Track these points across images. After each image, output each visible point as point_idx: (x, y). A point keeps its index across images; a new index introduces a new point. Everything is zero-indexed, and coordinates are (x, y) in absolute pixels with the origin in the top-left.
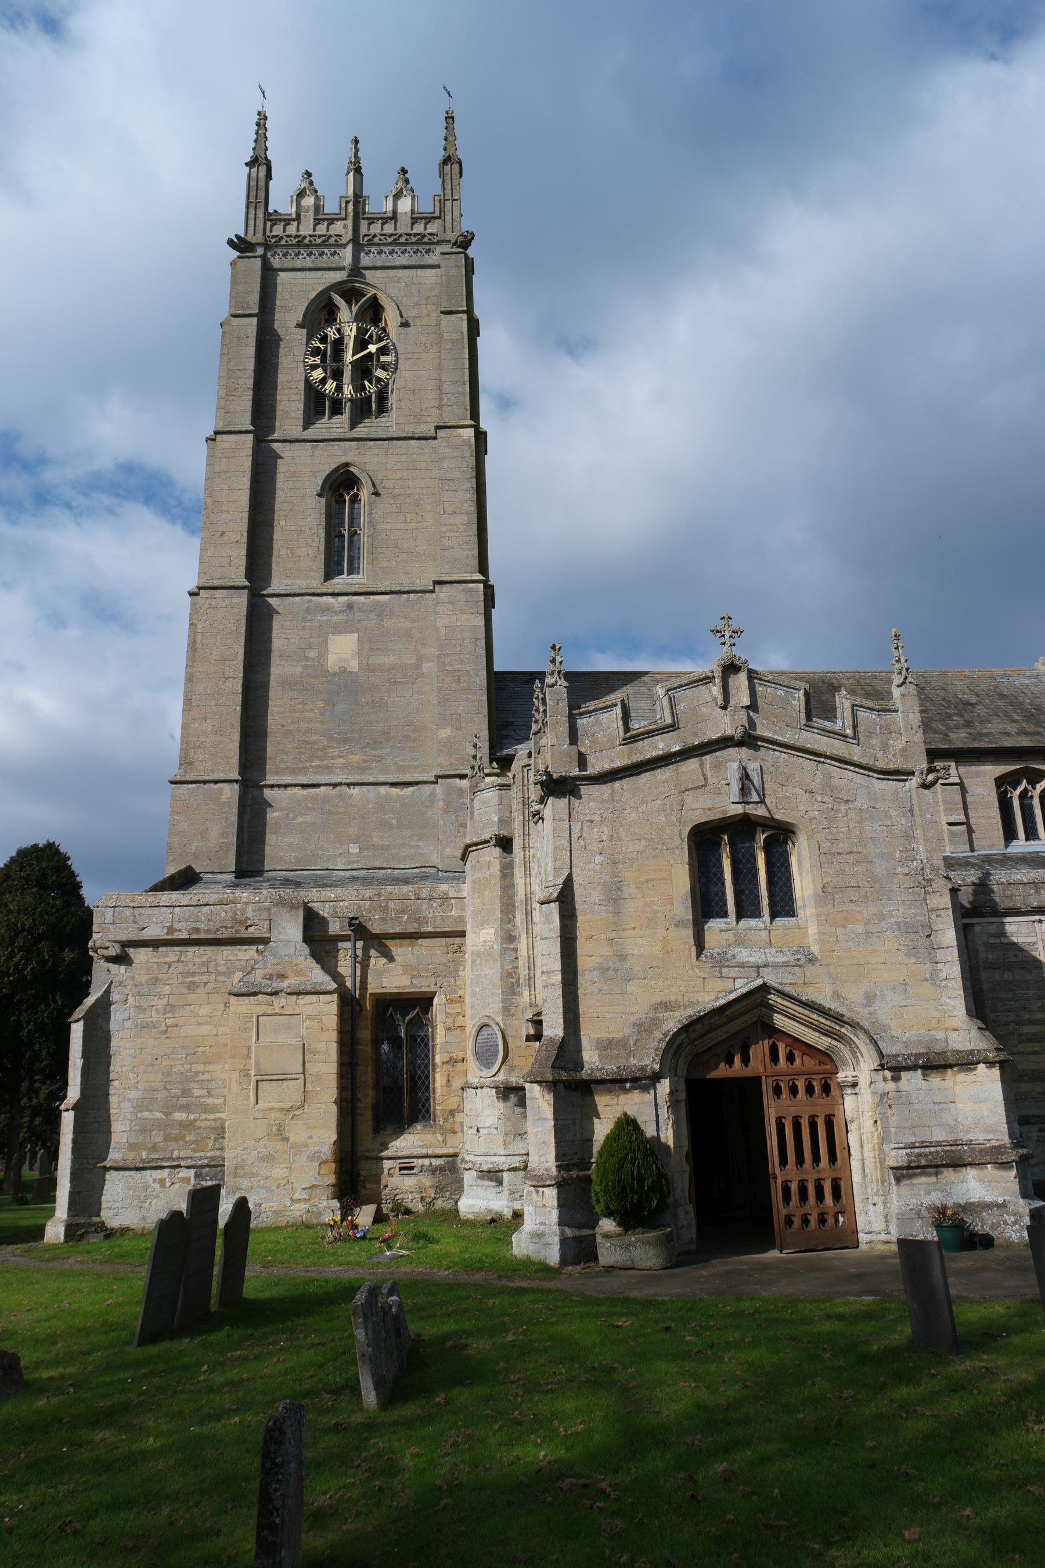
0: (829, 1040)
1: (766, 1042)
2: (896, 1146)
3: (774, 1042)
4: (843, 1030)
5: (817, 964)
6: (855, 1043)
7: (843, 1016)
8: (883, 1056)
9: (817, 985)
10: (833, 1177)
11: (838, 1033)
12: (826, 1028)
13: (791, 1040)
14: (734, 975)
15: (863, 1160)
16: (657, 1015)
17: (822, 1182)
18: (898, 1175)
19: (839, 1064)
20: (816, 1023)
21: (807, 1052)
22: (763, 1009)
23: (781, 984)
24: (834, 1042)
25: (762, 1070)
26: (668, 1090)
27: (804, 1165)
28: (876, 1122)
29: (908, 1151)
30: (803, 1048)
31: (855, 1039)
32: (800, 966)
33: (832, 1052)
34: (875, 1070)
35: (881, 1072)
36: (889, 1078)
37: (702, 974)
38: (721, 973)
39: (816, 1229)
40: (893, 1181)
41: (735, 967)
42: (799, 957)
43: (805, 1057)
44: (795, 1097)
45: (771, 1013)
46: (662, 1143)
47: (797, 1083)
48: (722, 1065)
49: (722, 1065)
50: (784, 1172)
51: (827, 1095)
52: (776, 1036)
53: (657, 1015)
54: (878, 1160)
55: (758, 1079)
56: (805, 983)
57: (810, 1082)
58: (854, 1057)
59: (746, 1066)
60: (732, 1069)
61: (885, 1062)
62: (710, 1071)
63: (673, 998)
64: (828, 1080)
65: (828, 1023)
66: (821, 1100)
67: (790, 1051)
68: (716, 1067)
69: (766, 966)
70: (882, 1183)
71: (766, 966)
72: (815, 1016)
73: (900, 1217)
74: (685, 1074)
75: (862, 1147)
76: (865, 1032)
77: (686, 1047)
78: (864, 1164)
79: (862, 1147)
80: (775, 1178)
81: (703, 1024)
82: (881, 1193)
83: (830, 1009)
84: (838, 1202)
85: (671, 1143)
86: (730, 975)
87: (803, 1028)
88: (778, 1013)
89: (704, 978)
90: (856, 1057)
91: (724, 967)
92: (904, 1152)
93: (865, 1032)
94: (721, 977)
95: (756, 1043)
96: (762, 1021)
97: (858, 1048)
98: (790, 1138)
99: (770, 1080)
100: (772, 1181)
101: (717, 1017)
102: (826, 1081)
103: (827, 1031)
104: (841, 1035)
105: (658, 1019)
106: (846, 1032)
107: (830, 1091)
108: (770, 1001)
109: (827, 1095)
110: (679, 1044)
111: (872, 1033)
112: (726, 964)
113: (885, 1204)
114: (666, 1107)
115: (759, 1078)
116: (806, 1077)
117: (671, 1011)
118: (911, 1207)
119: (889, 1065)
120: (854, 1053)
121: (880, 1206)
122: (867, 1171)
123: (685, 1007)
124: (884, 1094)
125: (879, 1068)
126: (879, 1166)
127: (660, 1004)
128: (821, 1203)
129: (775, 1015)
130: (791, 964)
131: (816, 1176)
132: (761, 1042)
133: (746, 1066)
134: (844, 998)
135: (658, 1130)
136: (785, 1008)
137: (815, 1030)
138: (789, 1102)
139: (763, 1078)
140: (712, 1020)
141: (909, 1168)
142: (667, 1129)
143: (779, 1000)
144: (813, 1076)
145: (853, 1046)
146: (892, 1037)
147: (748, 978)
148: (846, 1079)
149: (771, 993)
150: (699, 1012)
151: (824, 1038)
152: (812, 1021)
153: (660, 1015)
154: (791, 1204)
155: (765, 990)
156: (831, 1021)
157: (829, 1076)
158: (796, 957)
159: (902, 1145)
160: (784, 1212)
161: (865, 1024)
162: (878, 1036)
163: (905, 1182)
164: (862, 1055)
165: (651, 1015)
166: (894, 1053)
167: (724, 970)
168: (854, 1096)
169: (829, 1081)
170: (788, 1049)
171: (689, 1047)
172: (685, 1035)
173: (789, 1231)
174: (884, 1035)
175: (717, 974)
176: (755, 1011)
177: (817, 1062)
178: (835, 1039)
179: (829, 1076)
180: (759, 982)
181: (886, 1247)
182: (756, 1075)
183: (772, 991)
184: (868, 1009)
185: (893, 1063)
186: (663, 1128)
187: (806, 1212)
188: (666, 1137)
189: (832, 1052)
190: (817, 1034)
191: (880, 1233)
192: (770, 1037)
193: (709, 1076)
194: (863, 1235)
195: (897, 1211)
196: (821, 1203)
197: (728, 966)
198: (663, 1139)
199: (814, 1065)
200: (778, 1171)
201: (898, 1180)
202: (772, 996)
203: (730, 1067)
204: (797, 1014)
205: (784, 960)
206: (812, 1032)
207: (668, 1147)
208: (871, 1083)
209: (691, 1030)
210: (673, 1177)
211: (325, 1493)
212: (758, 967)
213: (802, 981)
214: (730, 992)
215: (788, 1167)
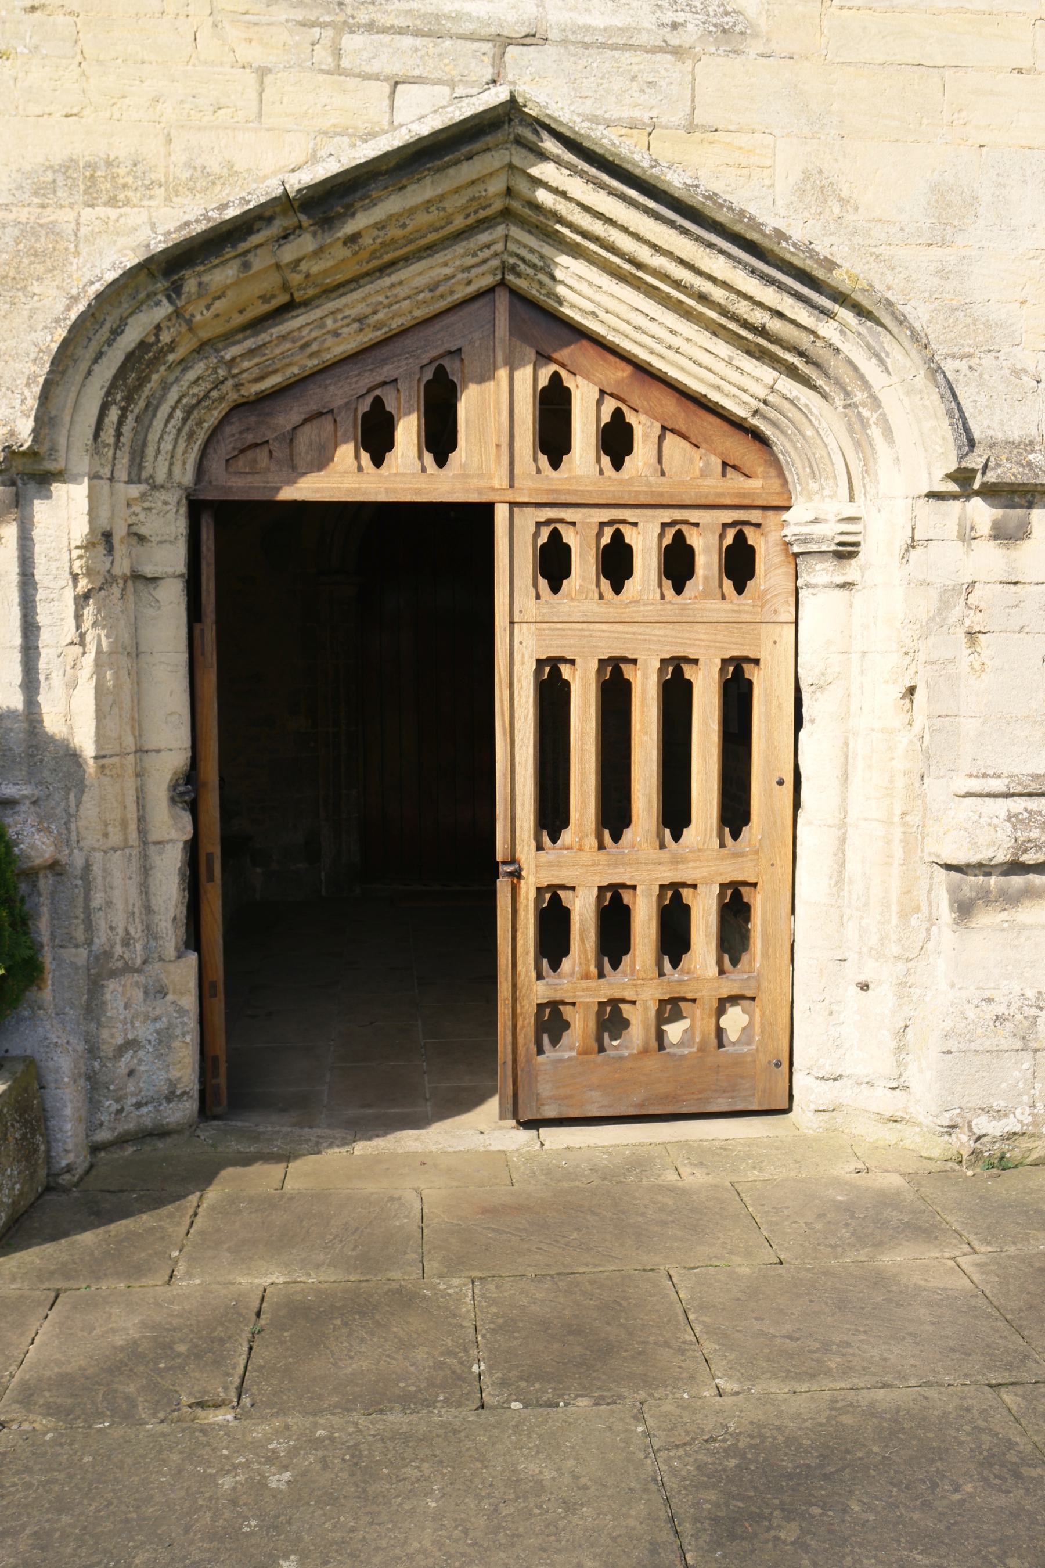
0: (767, 373)
1: (524, 375)
2: (976, 785)
3: (556, 377)
4: (827, 330)
5: (754, 47)
6: (866, 385)
7: (830, 265)
8: (972, 443)
9: (742, 140)
10: (727, 879)
11: (805, 341)
12: (759, 317)
13: (624, 372)
14: (396, 68)
15: (843, 825)
16: (50, 215)
17: (686, 893)
18: (967, 892)
19: (796, 469)
20: (718, 294)
21: (682, 427)
22: (516, 232)
23: (595, 120)
24: (787, 385)
25: (500, 480)
26: (80, 529)
27: (628, 834)
28: (912, 690)
29: (1018, 805)
30: (669, 404)
31: (869, 367)
32: (677, 52)
33: (774, 424)
34: (933, 495)
35: (956, 505)
36: (984, 528)
37: (255, 55)
38: (337, 52)
39: (645, 1051)
40: (945, 913)
41: (401, 31)
42: (680, 17)
43: (670, 438)
44: (617, 589)
45: (547, 250)
46: (51, 739)
47: (630, 536)
48: (345, 453)
49: (345, 453)
50: (551, 854)
51: (740, 589)
52: (564, 354)
53: (50, 215)
54: (898, 832)
55: (487, 510)
56: (691, 128)
57: (679, 536)
58: (858, 445)
59: (441, 461)
60: (384, 470)
61: (974, 462)
62: (295, 471)
63: (122, 149)
64: (749, 532)
65: (769, 295)
66: (718, 604)
67: (618, 414)
68: (322, 460)
69: (530, 39)
70: (904, 915)
71: (530, 39)
72: (718, 266)
73: (952, 1044)
74: (186, 475)
75: (845, 777)
76: (915, 337)
77: (184, 364)
78: (843, 841)
79: (845, 777)
80: (517, 875)
81: (246, 266)
82: (895, 950)
83: (780, 235)
84: (735, 962)
85: (85, 742)
86: (375, 67)
87: (671, 319)
88: (576, 251)
89: (263, 72)
90: (862, 445)
91: (353, 29)
92: (1003, 806)
93: (915, 337)
94: (338, 70)
95: (485, 376)
96: (515, 294)
97: (875, 402)
98: (583, 734)
99: (527, 520)
100: (503, 886)
101: (306, 243)
102: (740, 537)
103: (762, 331)
104: (818, 351)
105: (52, 230)
106: (836, 339)
107: (750, 573)
108: (542, 196)
109: (740, 589)
110: (143, 346)
111: (940, 350)
112: (363, 17)
113: (903, 985)
114: (69, 595)
115: (487, 510)
116: (667, 515)
117: (112, 202)
118: (1001, 1009)
119: (991, 477)
120: (857, 427)
121: (883, 994)
122: (853, 867)
123: (173, 190)
124: (955, 590)
125: (952, 487)
126: (898, 853)
127: (67, 167)
128: (675, 964)
129: (563, 259)
130: (643, 39)
131: (667, 876)
132: (503, 373)
133: (441, 461)
134: (844, 202)
135: (30, 683)
136: (597, 228)
137: (716, 330)
138: (592, 607)
139: (501, 513)
140: (288, 253)
141: (1016, 867)
142: (72, 684)
143: (576, 187)
144: (693, 516)
145: (859, 396)
146: (1016, 373)
147: (452, 84)
148: (817, 530)
149: (543, 156)
150: (224, 206)
151: (749, 364)
152: (707, 287)
153: (64, 217)
154: (566, 964)
155: (519, 142)
156: (781, 286)
157: (754, 516)
158: (669, 17)
159: (997, 785)
160: (539, 992)
161: (919, 314)
162: (963, 365)
163: (988, 918)
164: (888, 432)
165: (23, 215)
166: (1015, 435)
167: (352, 42)
168: (843, 593)
169: (752, 537)
170: (609, 406)
171: (199, 368)
172: (165, 309)
173: (551, 1054)
174: (988, 360)
175: (323, 56)
176: (484, 238)
177: (716, 463)
178: (792, 372)
179: (754, 516)
180: (498, 96)
181: (888, 1134)
182: (473, 498)
183: (550, 145)
184: (936, 252)
185: (1006, 472)
186: (57, 680)
187: (617, 995)
188: (68, 718)
189: (774, 424)
190: (723, 349)
191: (870, 1084)
192: (544, 357)
193: (287, 494)
194: (810, 1080)
195: (948, 1025)
196: (675, 964)
197: (371, 27)
198: (52, 723)
199: (703, 474)
200: (526, 850)
201: (964, 909)
202: (543, 171)
203: (378, 461)
204: (644, 254)
205: (618, 22)
206: (703, 338)
207: (74, 756)
208: (912, 545)
209: (190, 286)
210: (87, 867)
211: (59, 1037)
212: (503, 42)
213: (678, 116)
214: (371, 135)
215: (567, 836)
